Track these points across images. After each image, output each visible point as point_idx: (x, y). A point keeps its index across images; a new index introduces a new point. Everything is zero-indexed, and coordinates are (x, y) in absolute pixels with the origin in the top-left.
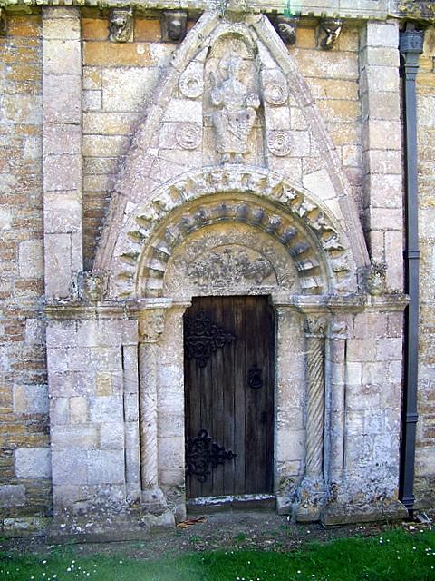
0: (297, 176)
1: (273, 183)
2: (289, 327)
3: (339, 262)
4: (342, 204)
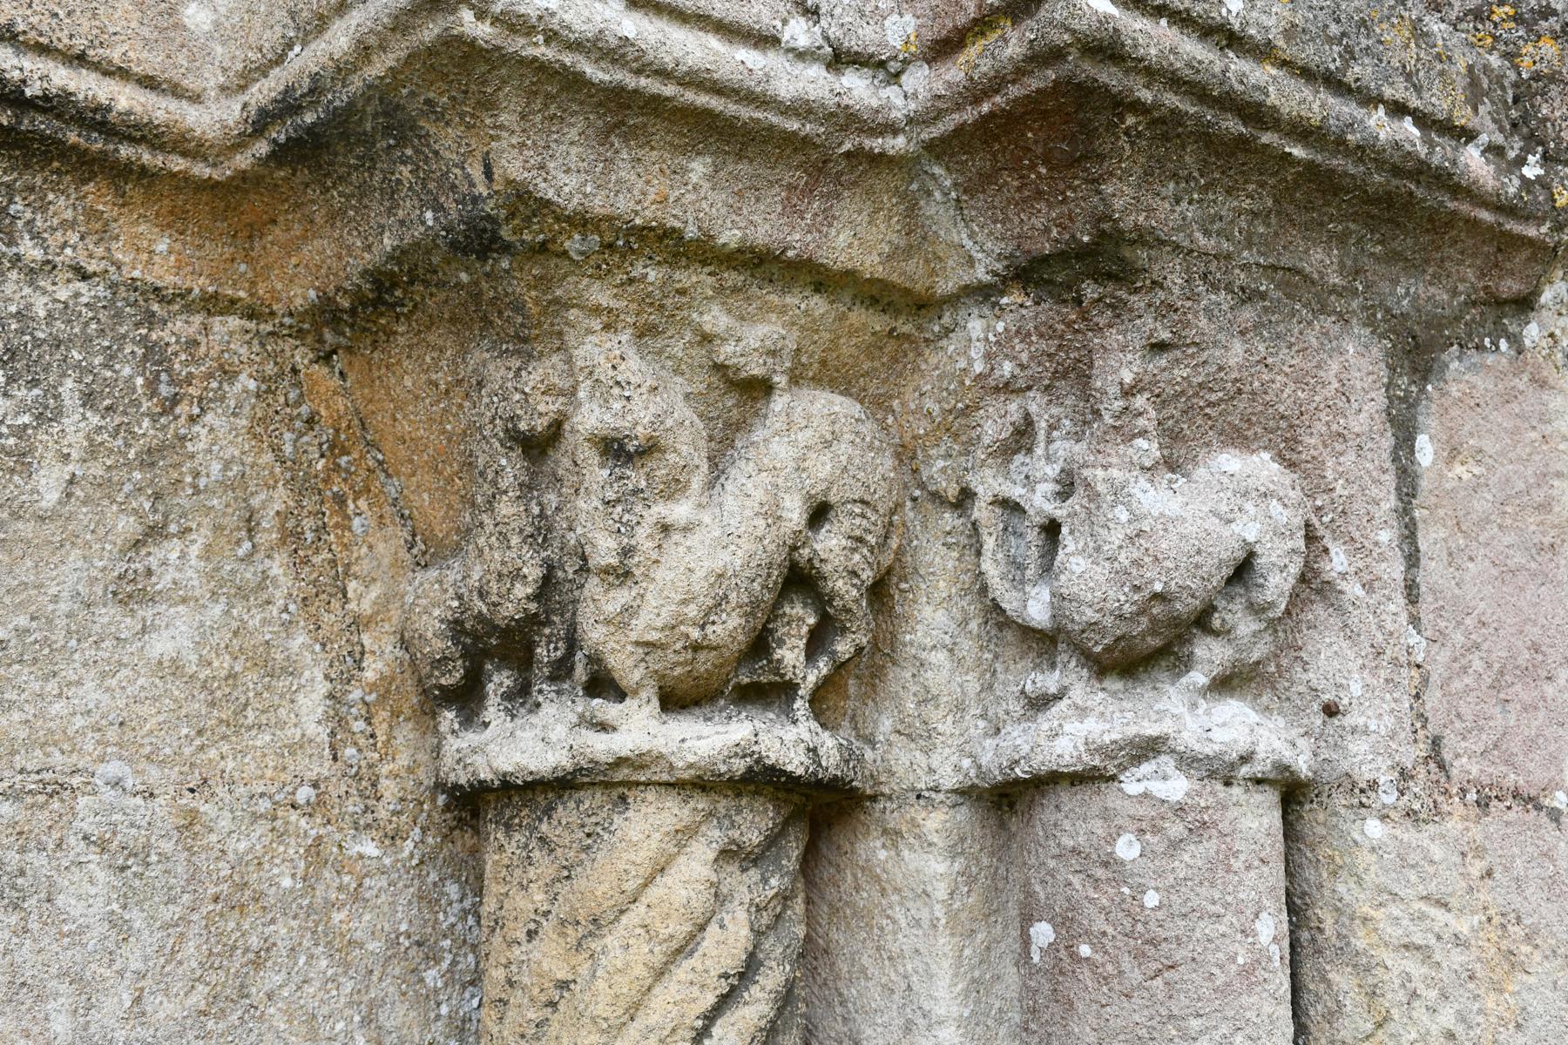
2: (132, 592)
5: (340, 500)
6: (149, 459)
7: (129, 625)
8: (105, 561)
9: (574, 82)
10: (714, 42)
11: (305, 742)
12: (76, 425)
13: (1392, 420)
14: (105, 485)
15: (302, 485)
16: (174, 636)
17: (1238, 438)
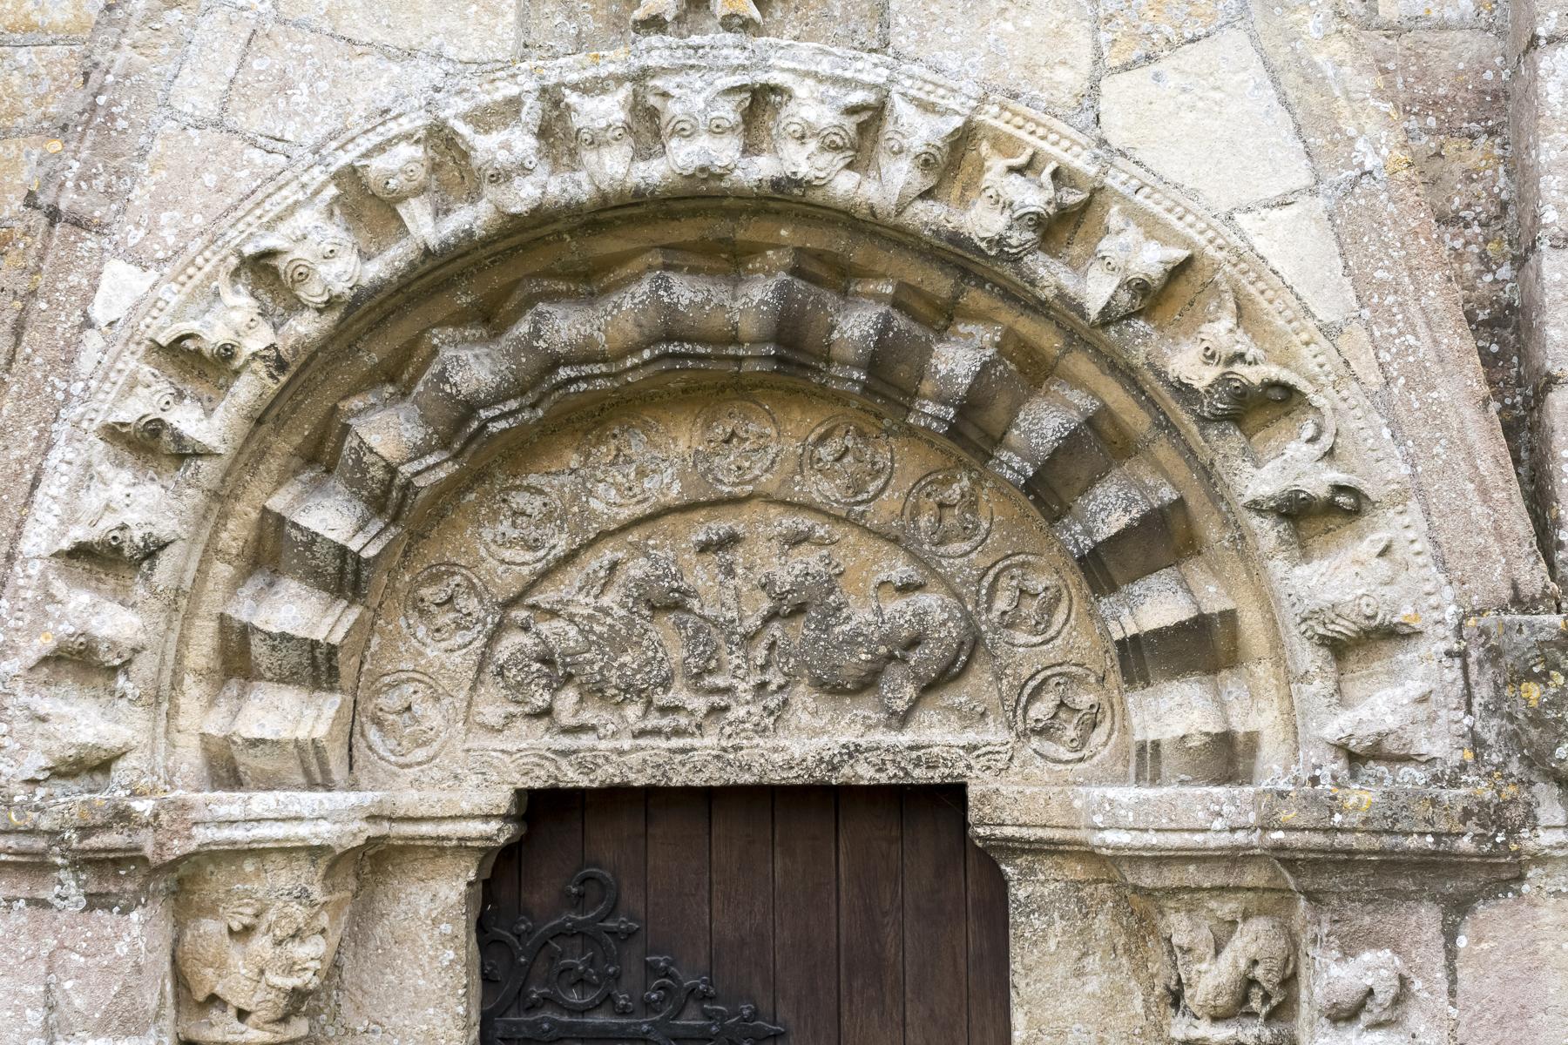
0: (1071, 79)
1: (917, 130)
2: (1079, 973)
3: (1338, 578)
4: (1346, 233)
5: (1144, 937)
6: (1081, 932)
7: (1078, 984)
8: (1070, 965)
9: (1142, 857)
10: (1186, 835)
11: (1137, 1015)
12: (1059, 925)
13: (1444, 933)
14: (1069, 943)
15: (1129, 932)
16: (1093, 985)
17: (1376, 945)
